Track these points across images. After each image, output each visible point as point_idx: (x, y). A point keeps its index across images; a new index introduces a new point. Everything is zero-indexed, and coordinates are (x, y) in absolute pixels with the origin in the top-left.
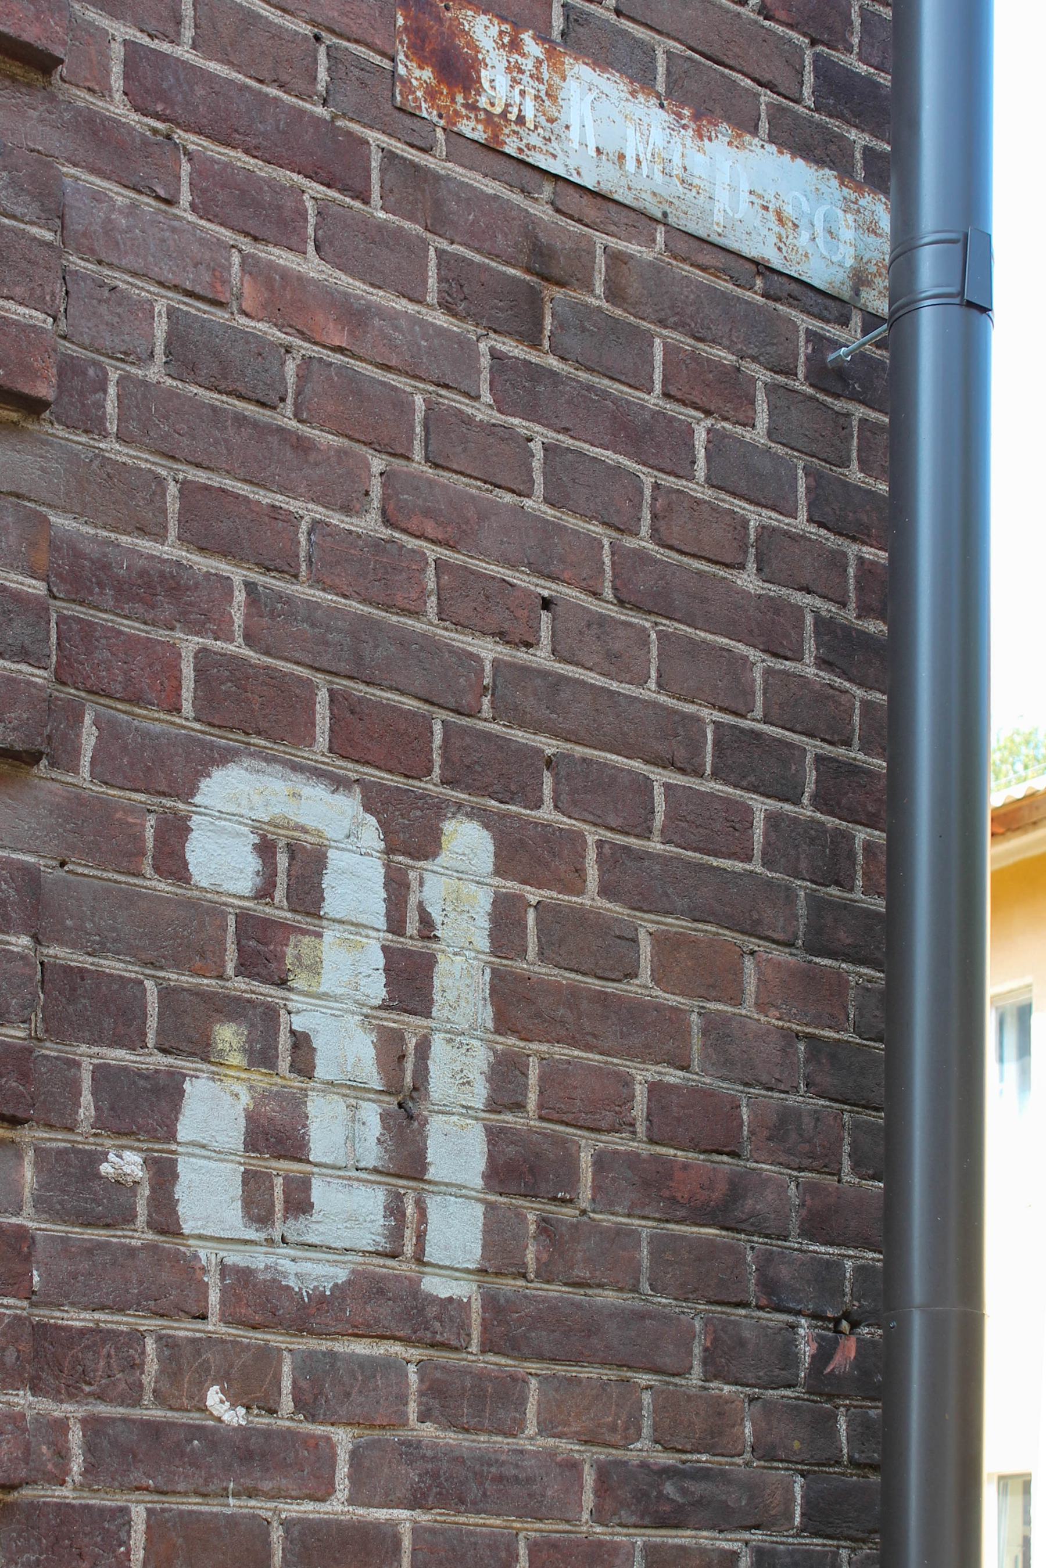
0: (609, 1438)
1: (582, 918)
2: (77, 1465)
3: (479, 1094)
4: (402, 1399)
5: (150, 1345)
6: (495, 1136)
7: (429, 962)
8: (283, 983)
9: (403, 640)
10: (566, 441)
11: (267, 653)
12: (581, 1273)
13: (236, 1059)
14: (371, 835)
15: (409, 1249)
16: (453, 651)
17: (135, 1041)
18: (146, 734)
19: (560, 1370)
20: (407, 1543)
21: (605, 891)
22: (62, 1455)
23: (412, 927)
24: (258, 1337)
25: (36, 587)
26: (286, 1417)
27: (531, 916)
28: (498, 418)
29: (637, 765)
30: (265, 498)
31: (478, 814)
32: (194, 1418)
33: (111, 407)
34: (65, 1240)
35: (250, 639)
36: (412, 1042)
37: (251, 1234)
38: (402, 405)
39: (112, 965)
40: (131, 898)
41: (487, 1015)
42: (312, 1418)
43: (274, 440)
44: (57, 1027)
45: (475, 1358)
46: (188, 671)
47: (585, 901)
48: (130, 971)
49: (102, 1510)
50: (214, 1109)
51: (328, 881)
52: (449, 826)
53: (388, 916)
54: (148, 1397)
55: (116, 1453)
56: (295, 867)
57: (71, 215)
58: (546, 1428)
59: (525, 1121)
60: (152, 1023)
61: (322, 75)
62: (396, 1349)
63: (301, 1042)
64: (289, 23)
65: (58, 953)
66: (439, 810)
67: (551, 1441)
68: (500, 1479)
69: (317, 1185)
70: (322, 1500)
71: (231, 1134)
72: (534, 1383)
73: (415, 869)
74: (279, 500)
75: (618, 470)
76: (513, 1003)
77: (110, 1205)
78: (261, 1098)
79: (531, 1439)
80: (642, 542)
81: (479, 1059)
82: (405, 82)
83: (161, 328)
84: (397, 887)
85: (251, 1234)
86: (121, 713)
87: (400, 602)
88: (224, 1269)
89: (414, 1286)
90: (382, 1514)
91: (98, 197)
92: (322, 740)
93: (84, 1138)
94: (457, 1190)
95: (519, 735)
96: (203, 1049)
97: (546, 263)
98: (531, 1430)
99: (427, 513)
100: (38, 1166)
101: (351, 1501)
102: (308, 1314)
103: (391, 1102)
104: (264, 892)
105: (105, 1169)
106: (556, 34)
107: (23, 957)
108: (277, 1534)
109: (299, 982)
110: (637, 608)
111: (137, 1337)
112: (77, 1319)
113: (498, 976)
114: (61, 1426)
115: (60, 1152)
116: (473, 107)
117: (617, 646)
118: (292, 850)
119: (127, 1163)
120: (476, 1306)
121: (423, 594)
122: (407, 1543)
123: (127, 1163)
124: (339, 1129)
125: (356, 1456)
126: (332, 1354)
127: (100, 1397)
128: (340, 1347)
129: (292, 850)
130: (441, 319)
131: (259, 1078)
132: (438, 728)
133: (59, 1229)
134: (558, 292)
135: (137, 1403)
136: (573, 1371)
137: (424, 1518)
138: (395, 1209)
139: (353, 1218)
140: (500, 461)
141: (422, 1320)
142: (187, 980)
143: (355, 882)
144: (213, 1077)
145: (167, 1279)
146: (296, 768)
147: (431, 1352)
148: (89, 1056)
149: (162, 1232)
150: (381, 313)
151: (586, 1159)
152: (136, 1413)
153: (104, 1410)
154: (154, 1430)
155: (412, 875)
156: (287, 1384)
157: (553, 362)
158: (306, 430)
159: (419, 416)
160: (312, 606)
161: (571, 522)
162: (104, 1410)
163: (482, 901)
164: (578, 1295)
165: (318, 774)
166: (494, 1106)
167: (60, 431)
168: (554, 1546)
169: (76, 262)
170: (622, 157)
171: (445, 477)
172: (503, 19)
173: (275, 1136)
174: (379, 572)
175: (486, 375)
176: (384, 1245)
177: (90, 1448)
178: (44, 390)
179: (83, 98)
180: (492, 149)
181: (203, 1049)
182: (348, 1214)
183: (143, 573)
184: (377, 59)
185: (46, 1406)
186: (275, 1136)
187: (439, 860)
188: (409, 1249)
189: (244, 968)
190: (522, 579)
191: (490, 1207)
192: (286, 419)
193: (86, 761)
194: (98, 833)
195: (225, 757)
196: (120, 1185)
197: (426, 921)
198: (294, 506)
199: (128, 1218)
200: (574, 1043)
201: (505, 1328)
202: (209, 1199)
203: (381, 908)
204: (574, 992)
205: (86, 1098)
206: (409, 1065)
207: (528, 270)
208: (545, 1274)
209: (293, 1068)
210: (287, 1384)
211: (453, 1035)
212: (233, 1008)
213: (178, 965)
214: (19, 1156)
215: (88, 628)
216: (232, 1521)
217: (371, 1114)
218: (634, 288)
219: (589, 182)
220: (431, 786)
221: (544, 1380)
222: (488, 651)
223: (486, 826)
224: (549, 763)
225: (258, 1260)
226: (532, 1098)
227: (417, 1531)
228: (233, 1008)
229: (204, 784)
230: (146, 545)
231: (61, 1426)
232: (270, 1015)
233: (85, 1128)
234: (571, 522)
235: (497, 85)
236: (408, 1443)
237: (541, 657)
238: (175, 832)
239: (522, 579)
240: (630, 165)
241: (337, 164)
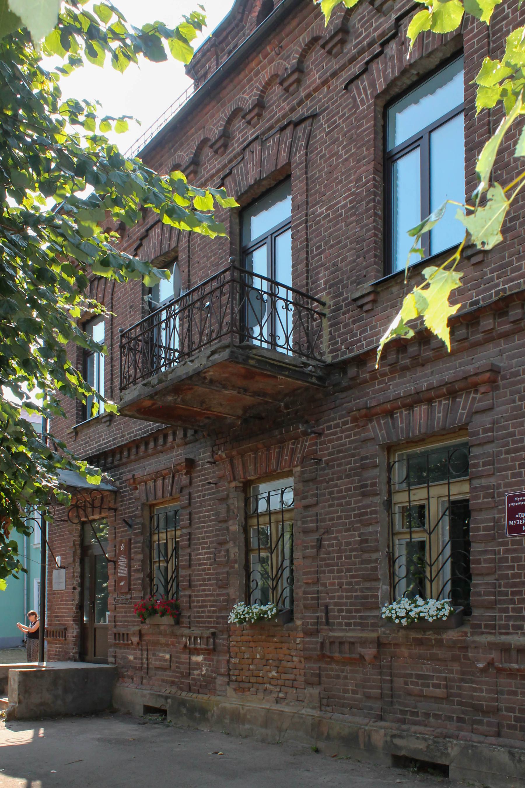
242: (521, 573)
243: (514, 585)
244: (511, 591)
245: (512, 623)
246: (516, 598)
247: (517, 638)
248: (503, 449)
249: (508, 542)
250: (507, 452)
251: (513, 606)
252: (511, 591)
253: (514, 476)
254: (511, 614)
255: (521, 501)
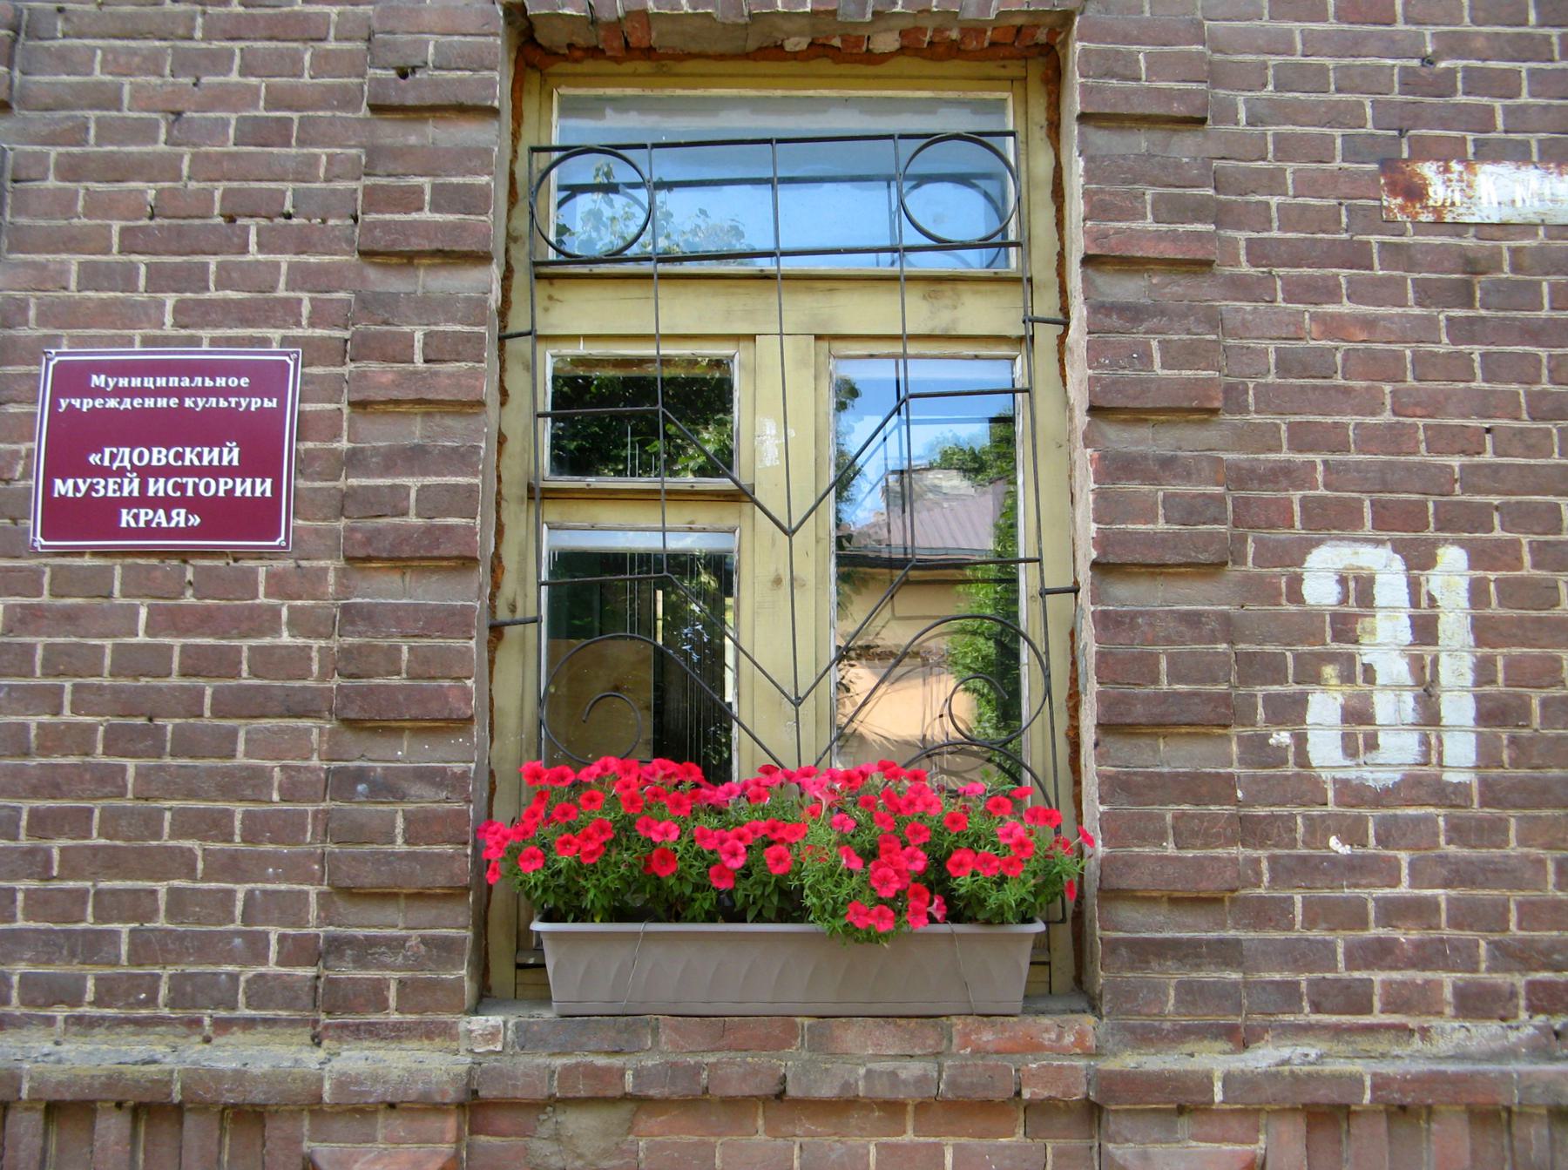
0: (1561, 845)
1: (1522, 582)
2: (1266, 877)
3: (1469, 678)
4: (1437, 835)
5: (1299, 820)
6: (1478, 699)
7: (1436, 618)
8: (1356, 642)
9: (1408, 468)
10: (1493, 348)
11: (1336, 490)
12: (1536, 761)
13: (1334, 681)
14: (1398, 563)
15: (1434, 760)
16: (1435, 466)
17: (1283, 680)
18: (1278, 541)
19: (1528, 812)
20: (1443, 906)
21: (1535, 565)
22: (1259, 874)
23: (1424, 602)
24: (1355, 811)
25: (1219, 490)
26: (1372, 847)
27: (1492, 587)
28: (1452, 348)
29: (1551, 498)
30: (1329, 420)
31: (1461, 544)
32: (1324, 852)
33: (1251, 399)
34: (1254, 776)
35: (1327, 486)
36: (1428, 659)
37: (1348, 763)
38: (1399, 357)
39: (1269, 648)
40: (1277, 615)
41: (1470, 639)
42: (1386, 847)
43: (1332, 393)
44: (1244, 680)
45: (1476, 810)
46: (1297, 508)
47: (1524, 573)
48: (1279, 649)
49: (1280, 898)
50: (1324, 706)
51: (1376, 590)
52: (1440, 551)
53: (1411, 601)
54: (1300, 844)
55: (1284, 871)
56: (1360, 588)
57: (1226, 322)
58: (1522, 842)
59: (1499, 687)
60: (1291, 671)
61: (1344, 220)
62: (1431, 810)
63: (1369, 670)
64: (1325, 202)
65: (1242, 647)
66: (1435, 544)
67: (1525, 850)
68: (1495, 871)
69: (1380, 735)
70: (1394, 887)
71: (1335, 716)
72: (1513, 821)
73: (1423, 576)
74: (1337, 419)
75: (1525, 355)
76: (1483, 631)
77: (1276, 757)
78: (1348, 698)
79: (1513, 849)
80: (1546, 385)
81: (1467, 661)
82: (1388, 209)
83: (1272, 358)
84: (1414, 587)
85: (1348, 763)
86: (1265, 534)
87: (1405, 449)
88: (1335, 781)
89: (1438, 779)
90: (1428, 892)
91: (1238, 310)
92: (1368, 523)
93: (1261, 728)
94: (1460, 728)
95: (1478, 498)
96: (1317, 679)
97: (1472, 265)
98: (1513, 843)
99: (1417, 404)
100: (1239, 745)
101: (1411, 886)
102: (1381, 797)
103: (1420, 690)
104: (1344, 600)
105: (1271, 741)
106: (1470, 156)
107: (1224, 653)
108: (1371, 905)
109: (1365, 639)
110: (1543, 419)
111: (1292, 817)
112: (1261, 811)
113: (1474, 618)
114: (1258, 861)
115: (1249, 737)
116: (1426, 207)
117: (1532, 441)
118: (1357, 579)
119: (1282, 737)
120: (1475, 784)
121: (1418, 442)
122: (1443, 906)
123: (1282, 737)
124: (1392, 706)
125: (1412, 865)
126: (1396, 816)
127: (1276, 846)
128: (1399, 812)
129: (1357, 579)
130: (1417, 311)
131: (1347, 689)
132: (1431, 506)
133: (1251, 771)
134: (1482, 278)
135: (1295, 847)
136: (1536, 812)
137: (1452, 893)
138: (1425, 742)
139: (1401, 749)
140: (1458, 367)
141: (1443, 794)
142: (1306, 648)
143: (1391, 585)
144: (1323, 692)
145: (1308, 788)
146: (1356, 540)
147: (1452, 810)
148: (1260, 691)
149: (1302, 766)
150: (1384, 318)
151: (1535, 704)
152: (1294, 852)
153: (1277, 852)
154: (1303, 860)
155: (1422, 579)
156: (1371, 832)
157: (1483, 312)
158: (1351, 383)
159: (1408, 360)
160: (1358, 463)
161: (1500, 387)
162: (1277, 852)
163: (1463, 584)
164: (1536, 773)
165: (1367, 540)
166: (1477, 683)
167: (1228, 417)
168: (1532, 903)
169: (1230, 342)
170: (1513, 202)
171: (1425, 385)
172: (1438, 160)
173: (1357, 715)
174: (1394, 438)
175: (1444, 331)
176: (1420, 759)
177: (1272, 870)
178: (1216, 404)
179: (1227, 270)
180: (1439, 222)
181: (1317, 679)
182: (1399, 749)
183: (1272, 469)
184: (1372, 203)
185: (1249, 852)
186: (1357, 715)
187: (1438, 568)
188: (1434, 760)
189: (1335, 638)
190: (1474, 422)
191: (1479, 734)
192: (1339, 380)
193: (1250, 559)
194: (1262, 590)
195: (1319, 543)
196: (1281, 749)
197: (1432, 600)
198: (1345, 419)
199: (1285, 762)
200: (1523, 645)
201: (1492, 793)
202: (1325, 749)
203: (1407, 597)
204: (1521, 619)
205: (1260, 710)
206: (1428, 671)
207: (1464, 272)
208: (1515, 764)
209: (1365, 681)
210: (1371, 832)
211: (1451, 652)
212: (1331, 658)
213: (1302, 642)
214: (1230, 741)
215: (1247, 500)
216: (1347, 900)
217: (1408, 699)
218: (1527, 261)
219: (1495, 220)
220: (1430, 533)
221: (1519, 819)
222: (1456, 462)
223: (1462, 547)
224: (1497, 508)
225: (1352, 774)
226: (1501, 677)
227: (1449, 900)
228: (1331, 658)
229: (1309, 558)
230: (1272, 456)
231: (1258, 861)
232: (1351, 658)
233: (1261, 724)
234: (1500, 387)
235: (1438, 192)
236: (1440, 856)
237: (1488, 457)
238: (1296, 582)
239: (1474, 422)
240: (1519, 204)
241: (1356, 256)
242: (92, 728)
243: (51, 784)
244: (34, 813)
245: (22, 968)
246: (56, 845)
247: (48, 1047)
248: (54, 152)
249: (37, 573)
250: (72, 170)
251: (34, 884)
252: (34, 813)
253: (92, 277)
254: (20, 924)
255: (119, 393)
